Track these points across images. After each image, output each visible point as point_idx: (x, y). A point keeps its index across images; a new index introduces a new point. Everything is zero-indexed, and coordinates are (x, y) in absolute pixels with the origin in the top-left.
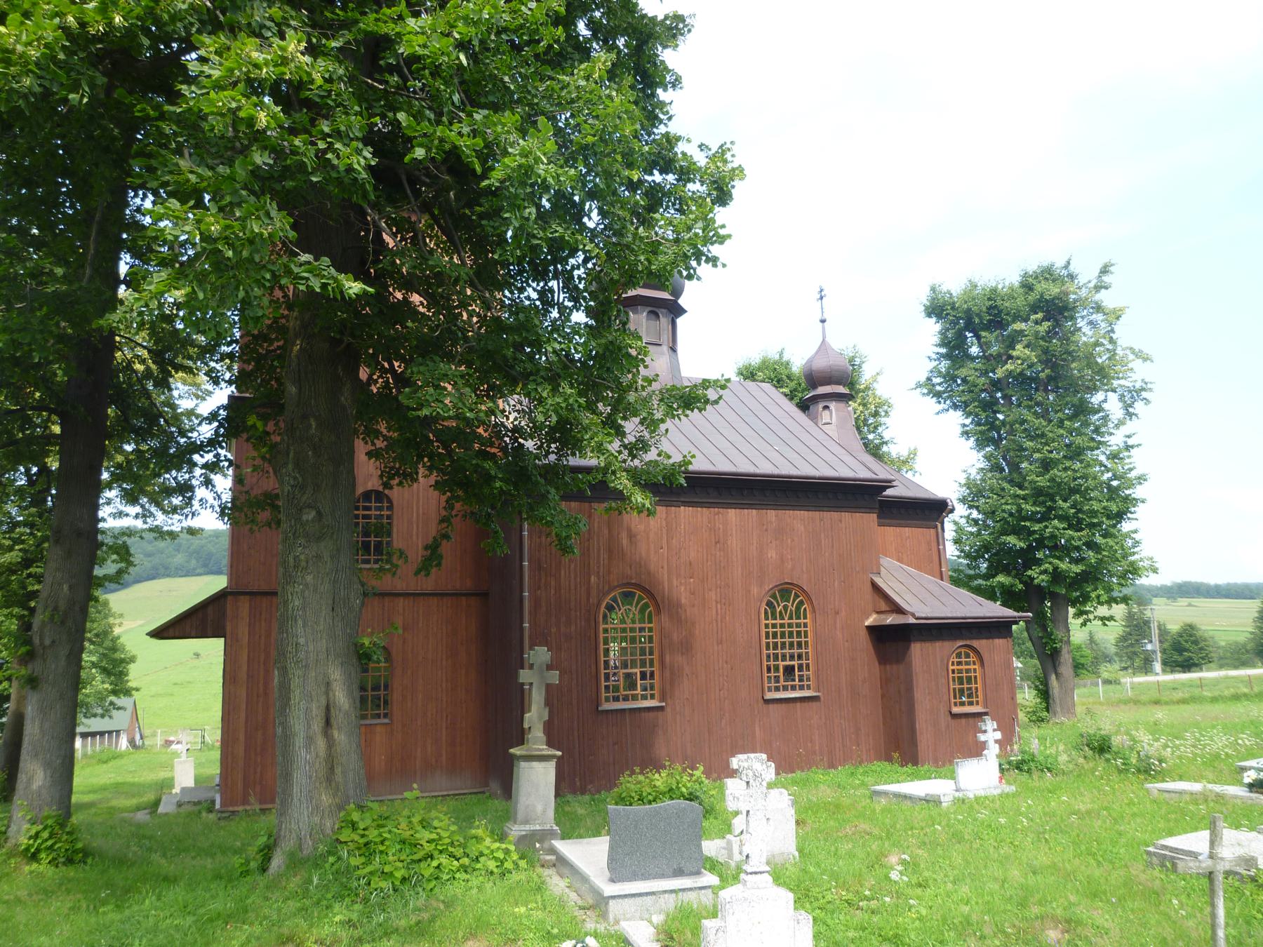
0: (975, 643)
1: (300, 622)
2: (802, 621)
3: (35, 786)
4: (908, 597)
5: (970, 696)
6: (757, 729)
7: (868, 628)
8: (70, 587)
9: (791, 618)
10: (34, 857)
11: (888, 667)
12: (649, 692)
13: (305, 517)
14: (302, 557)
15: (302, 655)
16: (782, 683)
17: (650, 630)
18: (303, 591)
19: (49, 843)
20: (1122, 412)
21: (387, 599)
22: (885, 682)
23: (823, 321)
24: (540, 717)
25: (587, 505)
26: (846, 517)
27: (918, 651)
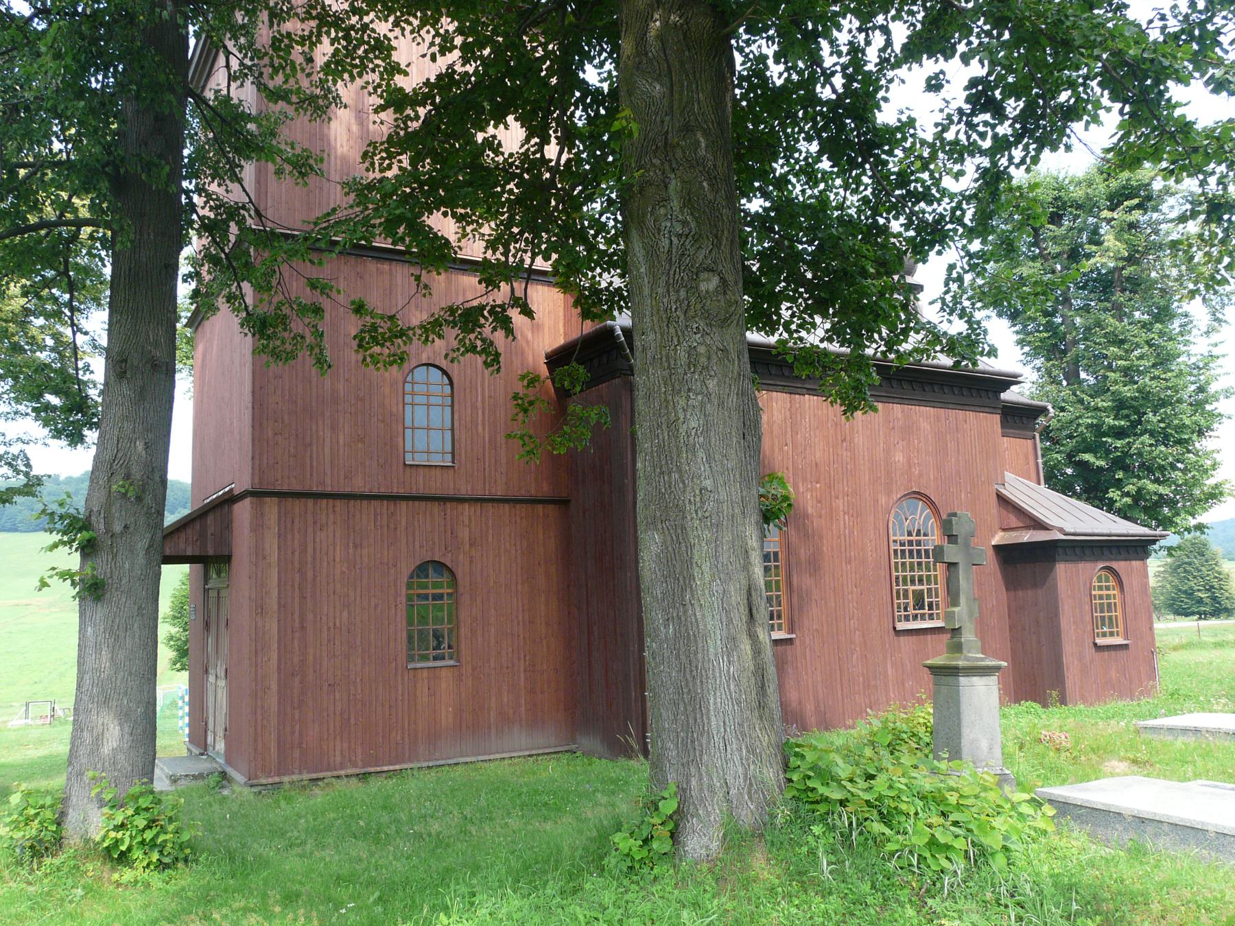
1: (701, 454)
3: (106, 750)
4: (1042, 510)
5: (1111, 626)
6: (889, 666)
7: (996, 547)
8: (147, 446)
10: (124, 859)
11: (1020, 593)
13: (703, 287)
14: (702, 349)
15: (710, 506)
16: (911, 611)
18: (702, 404)
19: (148, 835)
20: (1209, 316)
21: (448, 505)
22: (1015, 612)
24: (971, 614)
26: (971, 415)
27: (1063, 571)
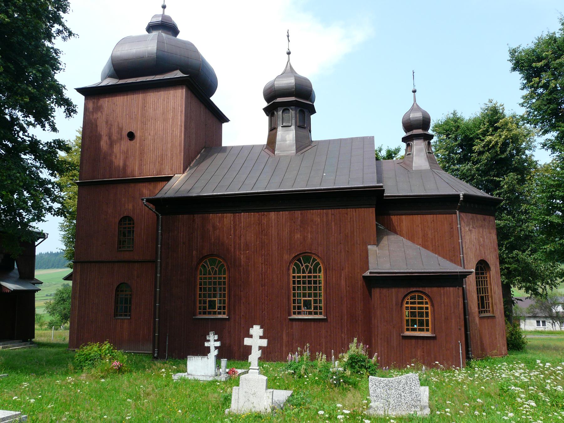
0: (427, 290)
2: (318, 274)
9: (310, 272)
12: (222, 311)
16: (303, 309)
17: (224, 278)
23: (414, 91)
25: (192, 216)
